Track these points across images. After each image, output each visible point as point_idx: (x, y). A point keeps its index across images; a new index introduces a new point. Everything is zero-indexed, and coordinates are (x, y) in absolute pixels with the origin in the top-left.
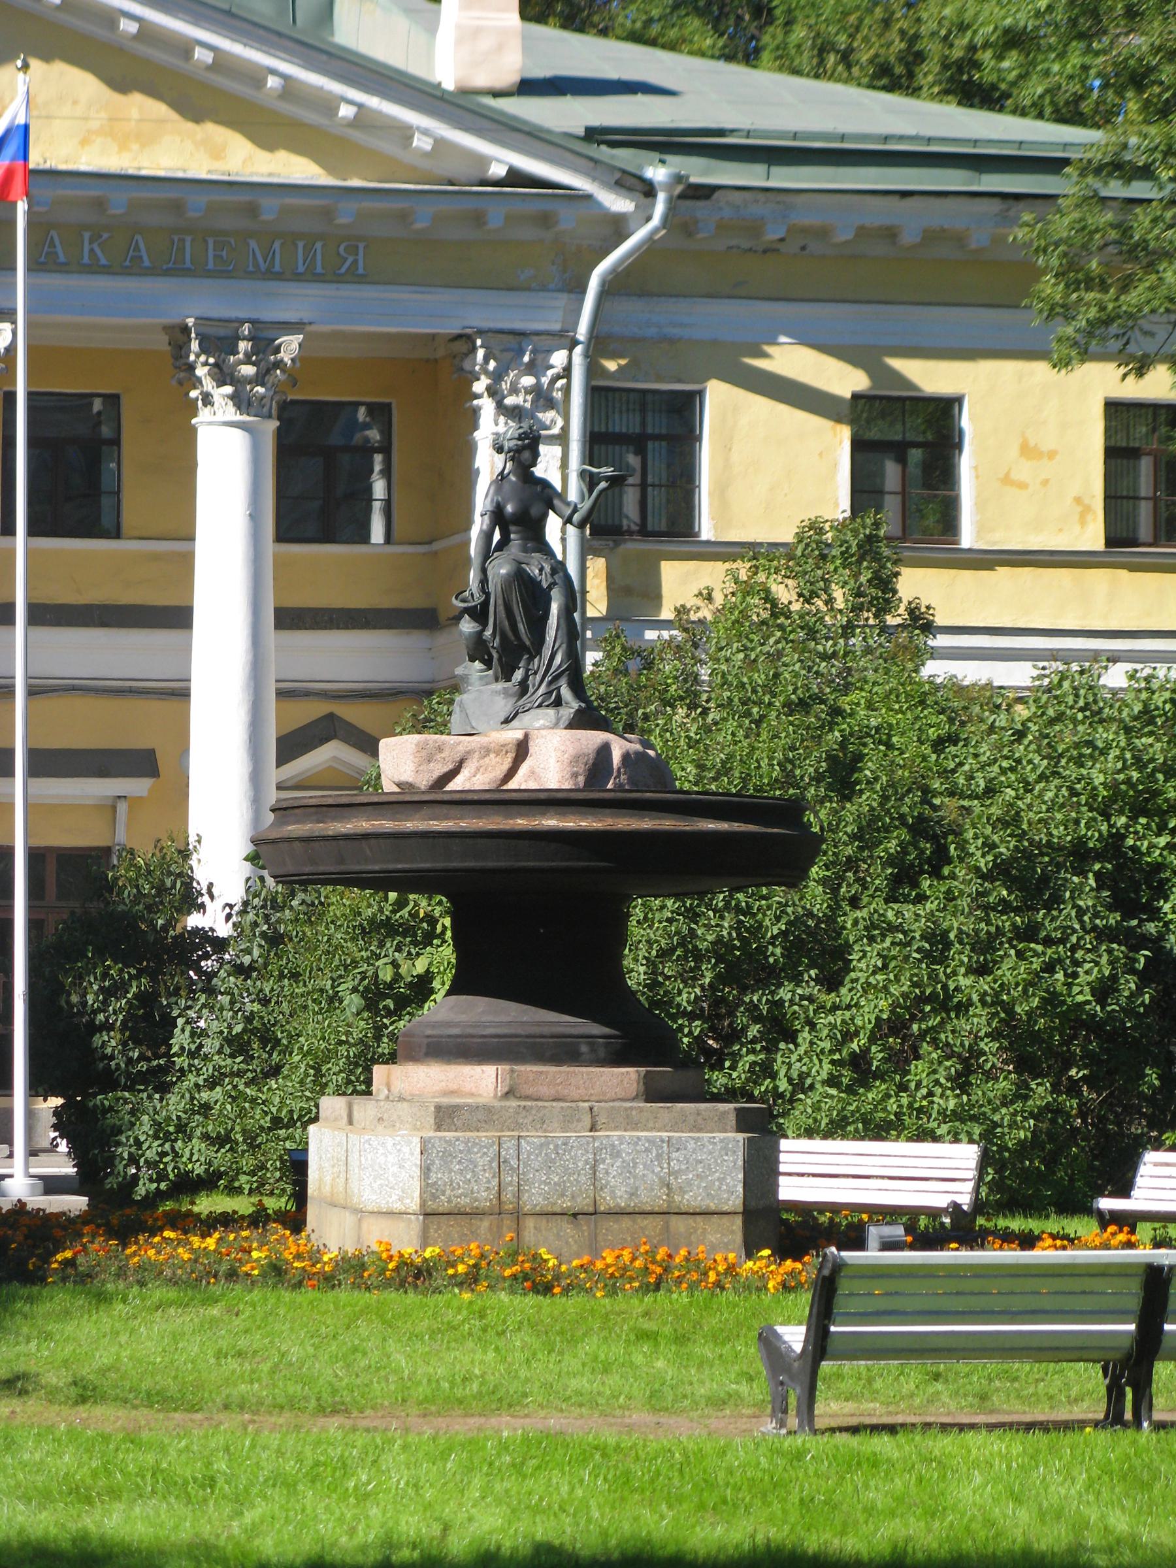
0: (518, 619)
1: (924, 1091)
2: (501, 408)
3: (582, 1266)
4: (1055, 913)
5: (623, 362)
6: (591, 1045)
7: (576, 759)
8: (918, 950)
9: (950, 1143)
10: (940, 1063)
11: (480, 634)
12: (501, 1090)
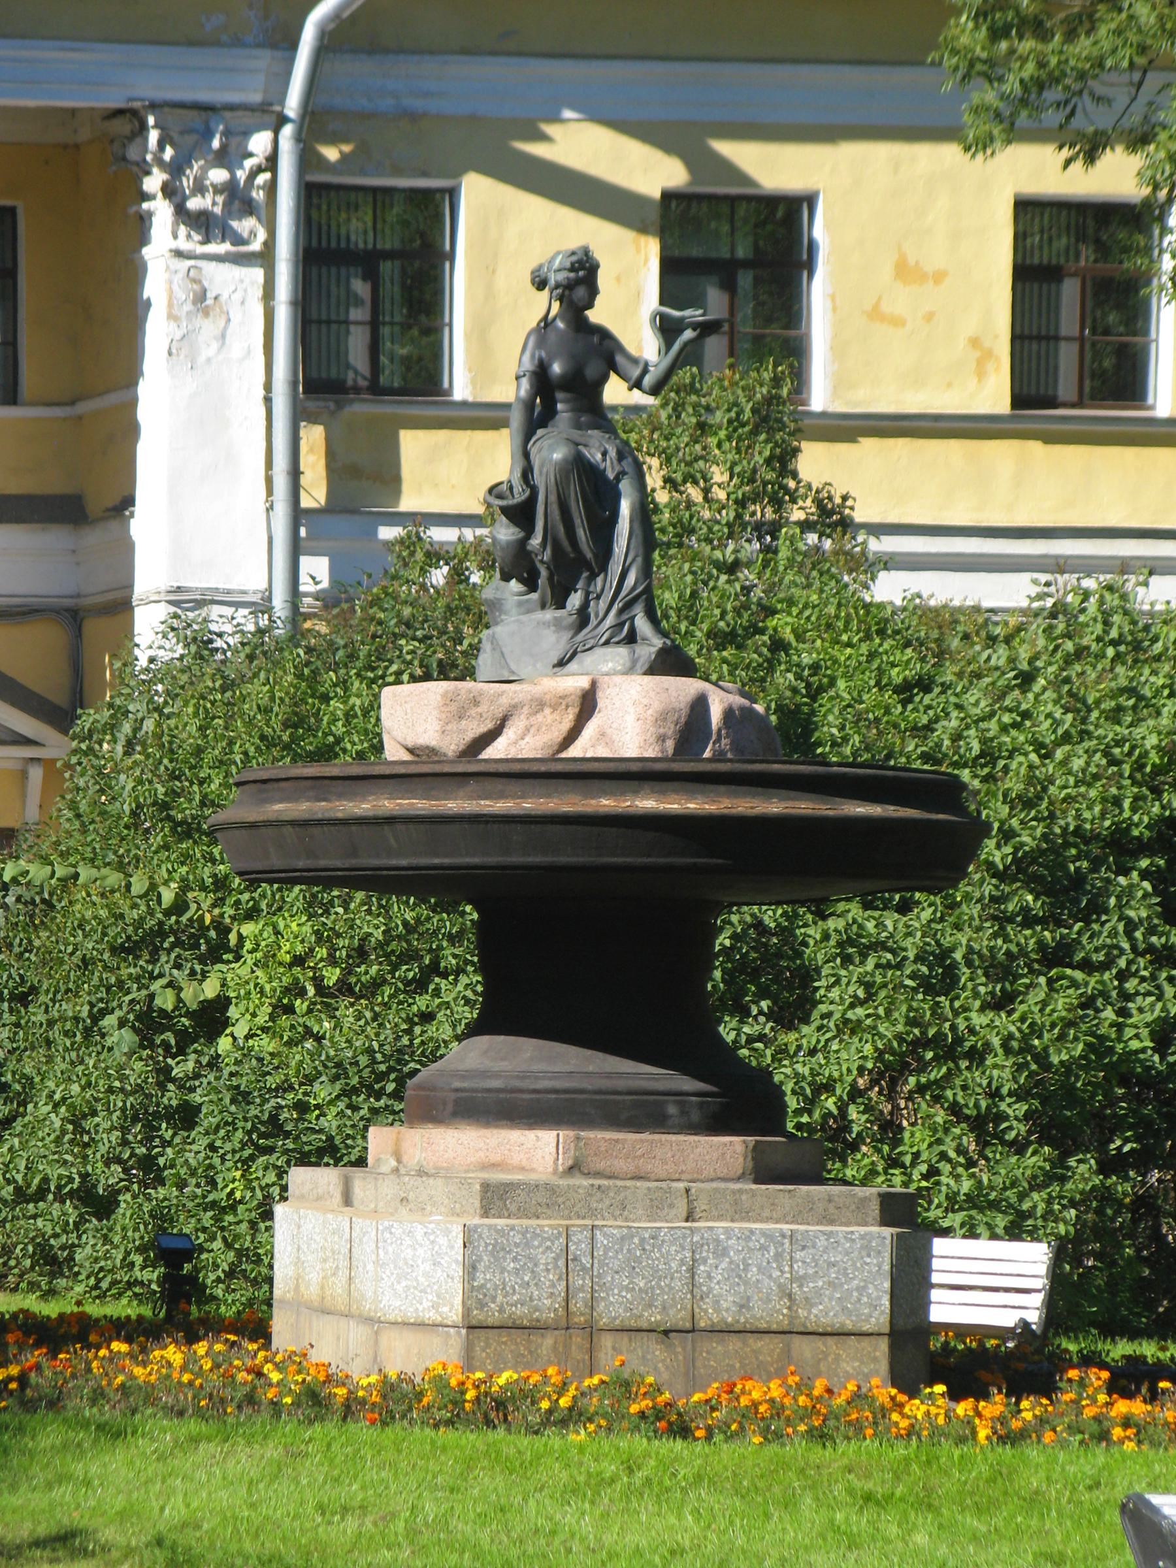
0: (578, 522)
1: (924, 1168)
2: (181, 212)
3: (707, 1401)
4: (1096, 927)
5: (347, 148)
6: (681, 1104)
7: (662, 717)
8: (913, 976)
9: (964, 1237)
10: (946, 1131)
11: (522, 543)
12: (563, 1163)
